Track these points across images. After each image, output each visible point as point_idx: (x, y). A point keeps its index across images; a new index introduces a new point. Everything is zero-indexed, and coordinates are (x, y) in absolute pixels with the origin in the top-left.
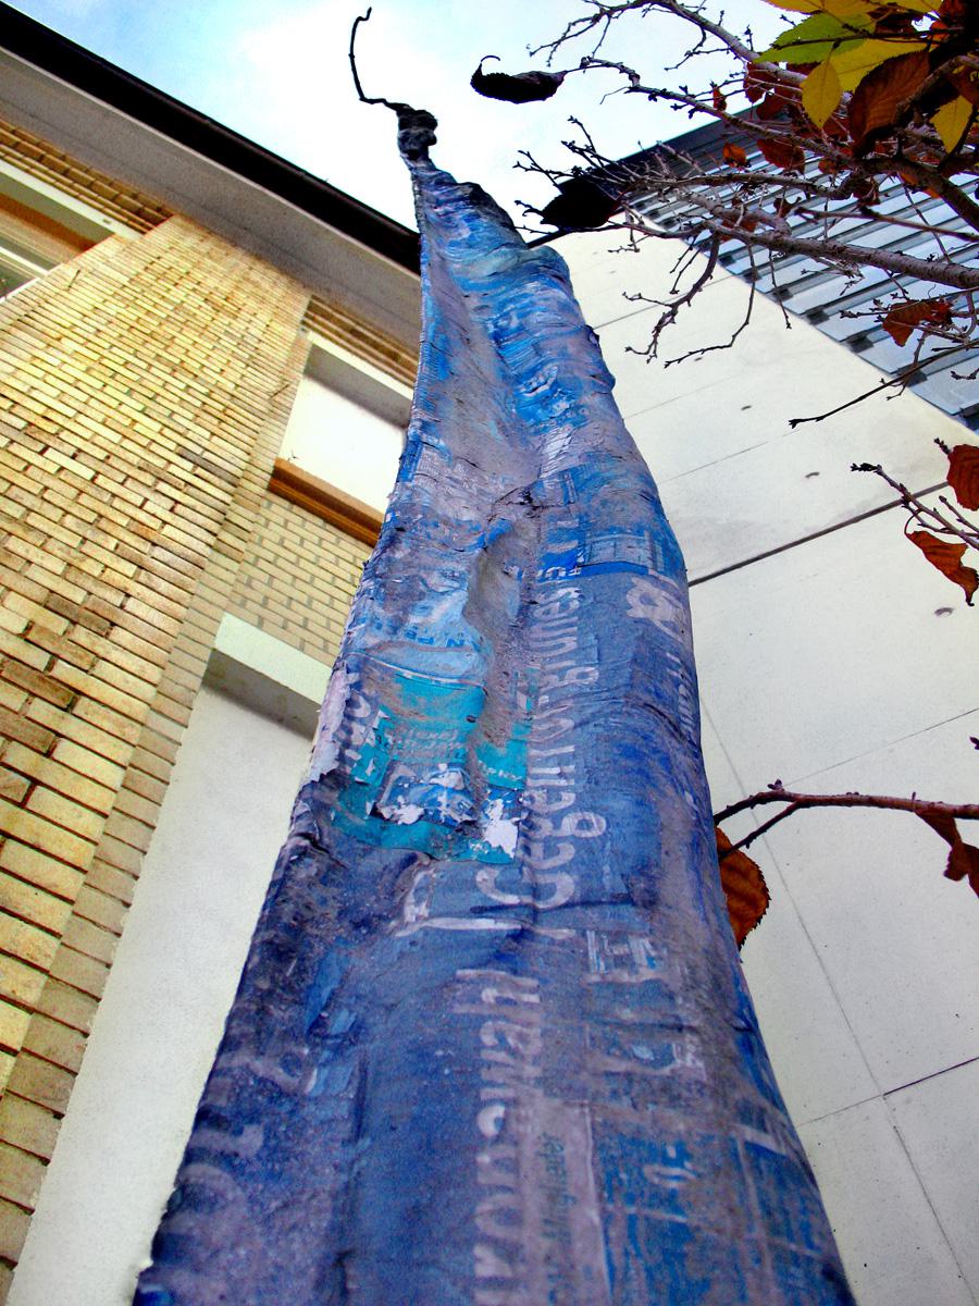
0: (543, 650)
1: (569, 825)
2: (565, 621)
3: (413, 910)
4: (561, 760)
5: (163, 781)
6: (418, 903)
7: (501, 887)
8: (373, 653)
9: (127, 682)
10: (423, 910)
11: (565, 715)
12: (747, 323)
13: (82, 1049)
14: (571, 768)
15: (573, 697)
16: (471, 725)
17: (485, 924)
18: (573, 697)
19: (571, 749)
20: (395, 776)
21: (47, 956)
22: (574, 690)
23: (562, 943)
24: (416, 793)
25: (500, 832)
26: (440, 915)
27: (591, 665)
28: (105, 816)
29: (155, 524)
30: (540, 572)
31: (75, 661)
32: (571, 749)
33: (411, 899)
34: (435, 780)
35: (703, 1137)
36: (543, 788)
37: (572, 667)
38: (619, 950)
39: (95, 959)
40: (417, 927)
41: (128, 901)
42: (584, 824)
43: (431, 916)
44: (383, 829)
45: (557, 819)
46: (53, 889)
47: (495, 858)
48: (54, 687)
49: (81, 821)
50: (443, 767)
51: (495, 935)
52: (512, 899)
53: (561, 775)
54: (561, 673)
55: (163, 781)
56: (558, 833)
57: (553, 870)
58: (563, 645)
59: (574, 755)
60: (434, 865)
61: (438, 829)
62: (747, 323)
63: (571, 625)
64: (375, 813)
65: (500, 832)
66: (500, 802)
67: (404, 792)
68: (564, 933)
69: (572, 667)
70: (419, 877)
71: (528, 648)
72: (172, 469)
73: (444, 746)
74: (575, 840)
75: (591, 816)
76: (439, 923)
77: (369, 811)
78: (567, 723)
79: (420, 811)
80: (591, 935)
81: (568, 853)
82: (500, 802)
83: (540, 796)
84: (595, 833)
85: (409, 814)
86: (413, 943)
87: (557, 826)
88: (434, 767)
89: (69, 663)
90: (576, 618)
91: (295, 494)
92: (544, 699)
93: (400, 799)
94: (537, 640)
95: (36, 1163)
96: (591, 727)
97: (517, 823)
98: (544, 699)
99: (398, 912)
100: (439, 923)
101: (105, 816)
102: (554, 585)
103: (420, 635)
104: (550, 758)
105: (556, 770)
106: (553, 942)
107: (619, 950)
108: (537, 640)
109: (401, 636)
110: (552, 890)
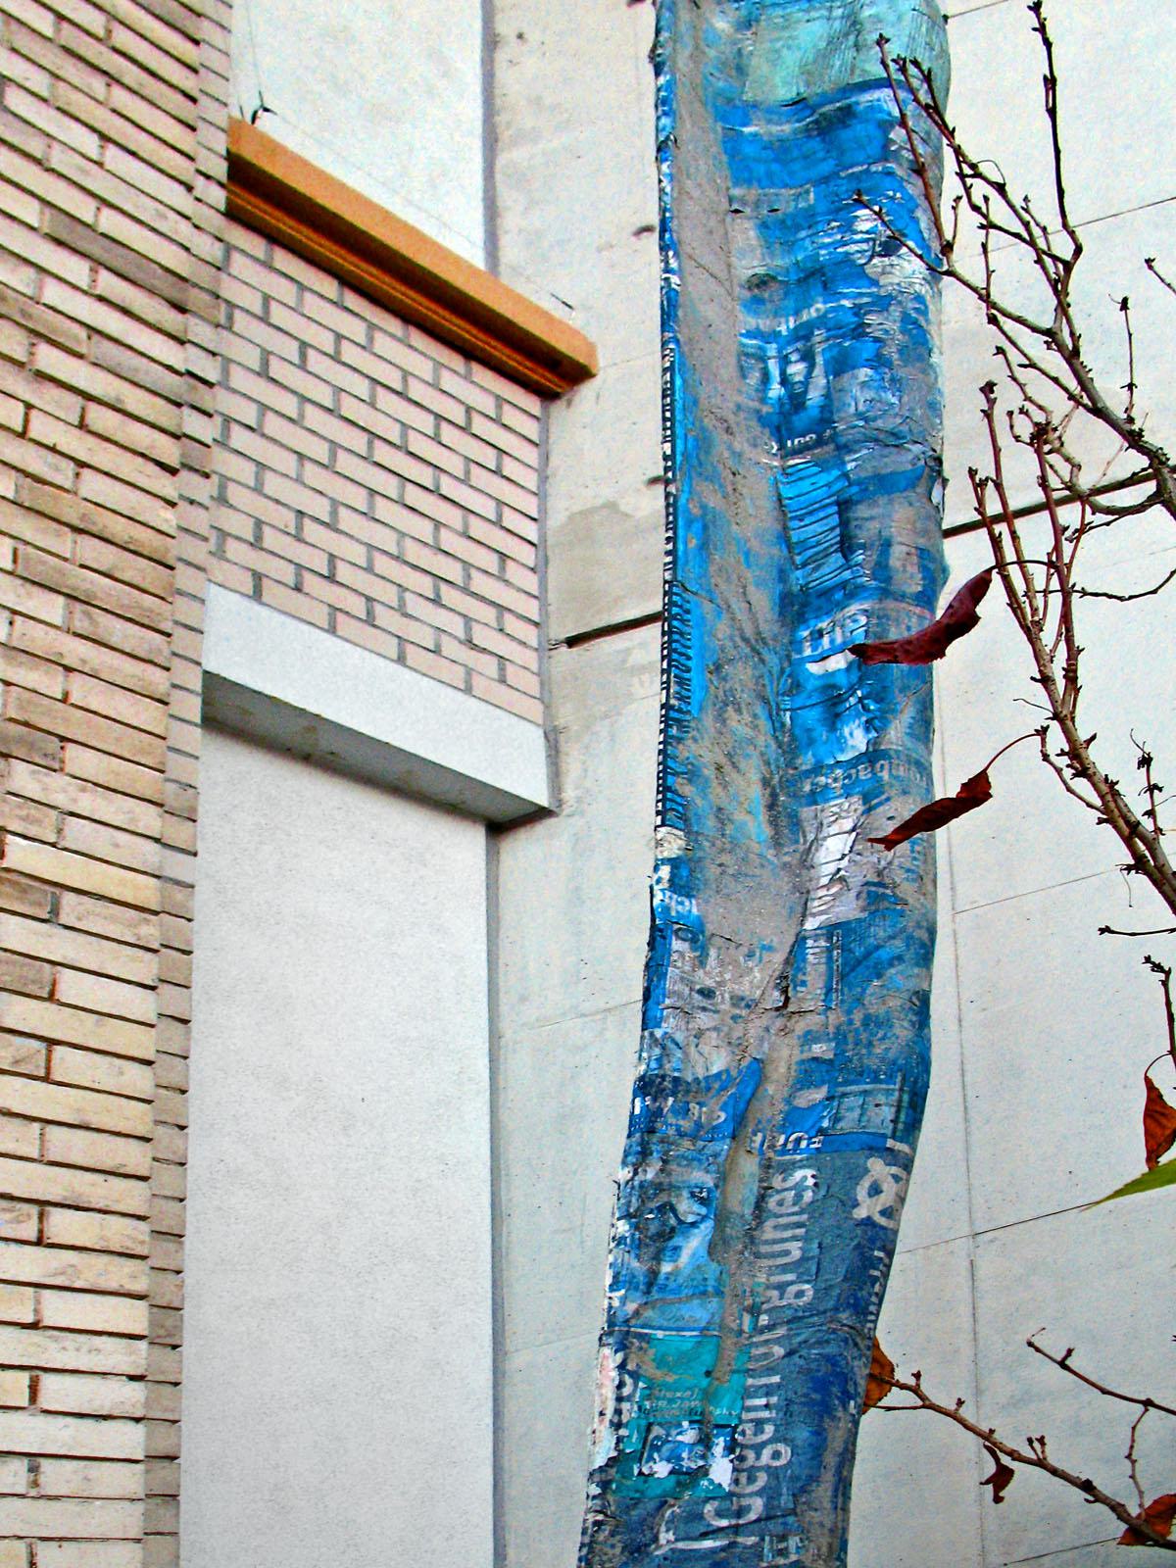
0: (773, 1255)
1: (766, 1457)
2: (795, 1219)
3: (666, 1536)
4: (769, 1391)
5: (184, 952)
6: (667, 1531)
7: (719, 1514)
8: (633, 1322)
9: (117, 846)
10: (671, 1536)
11: (777, 1341)
12: (1154, 592)
13: (180, 1286)
14: (774, 1400)
15: (789, 1322)
16: (525, 30)
17: (708, 1544)
18: (789, 1322)
19: (776, 1379)
20: (651, 1437)
21: (142, 1242)
22: (789, 1313)
23: (751, 1546)
24: (666, 1449)
25: (721, 1471)
26: (683, 1539)
27: (808, 1282)
28: (149, 1063)
29: (64, 474)
30: (782, 1139)
31: (32, 831)
32: (776, 1379)
33: (663, 1528)
34: (679, 1438)
35: (817, 223)
36: (752, 1421)
37: (792, 1283)
38: (782, 1546)
39: (166, 1197)
40: (667, 1548)
41: (182, 1123)
42: (776, 1455)
43: (677, 1540)
44: (645, 1482)
45: (758, 1449)
46: (121, 1171)
47: (717, 1494)
48: (24, 890)
49: (126, 1078)
50: (685, 1424)
51: (713, 1551)
52: (724, 1523)
53: (767, 1406)
54: (781, 1288)
55: (184, 952)
56: (758, 1464)
57: (751, 1495)
58: (787, 1253)
59: (779, 1386)
60: (678, 1503)
61: (682, 1477)
62: (1154, 592)
63: (799, 1225)
64: (641, 1473)
65: (721, 1471)
66: (722, 1439)
67: (658, 1449)
68: (752, 1540)
69: (792, 1283)
70: (668, 1513)
71: (758, 1256)
72: (53, 294)
73: (687, 1405)
74: (768, 1468)
75: (781, 1447)
76: (681, 1545)
77: (636, 1472)
78: (779, 1351)
79: (671, 1466)
80: (767, 1538)
81: (762, 1479)
82: (722, 1439)
83: (749, 1428)
84: (782, 1462)
85: (662, 1469)
86: (665, 1559)
87: (758, 1457)
88: (680, 1425)
89: (25, 837)
90: (805, 1217)
91: (286, 225)
92: (764, 1320)
93: (656, 1455)
94: (766, 1242)
95: (170, 1388)
96: (796, 1358)
97: (732, 1461)
98: (764, 1320)
99: (656, 1539)
100: (681, 1545)
101: (149, 1063)
102: (794, 1163)
103: (672, 1285)
104: (761, 1387)
105: (763, 1401)
106: (746, 1547)
107: (782, 1546)
108: (766, 1242)
109: (655, 1295)
110: (748, 1509)
